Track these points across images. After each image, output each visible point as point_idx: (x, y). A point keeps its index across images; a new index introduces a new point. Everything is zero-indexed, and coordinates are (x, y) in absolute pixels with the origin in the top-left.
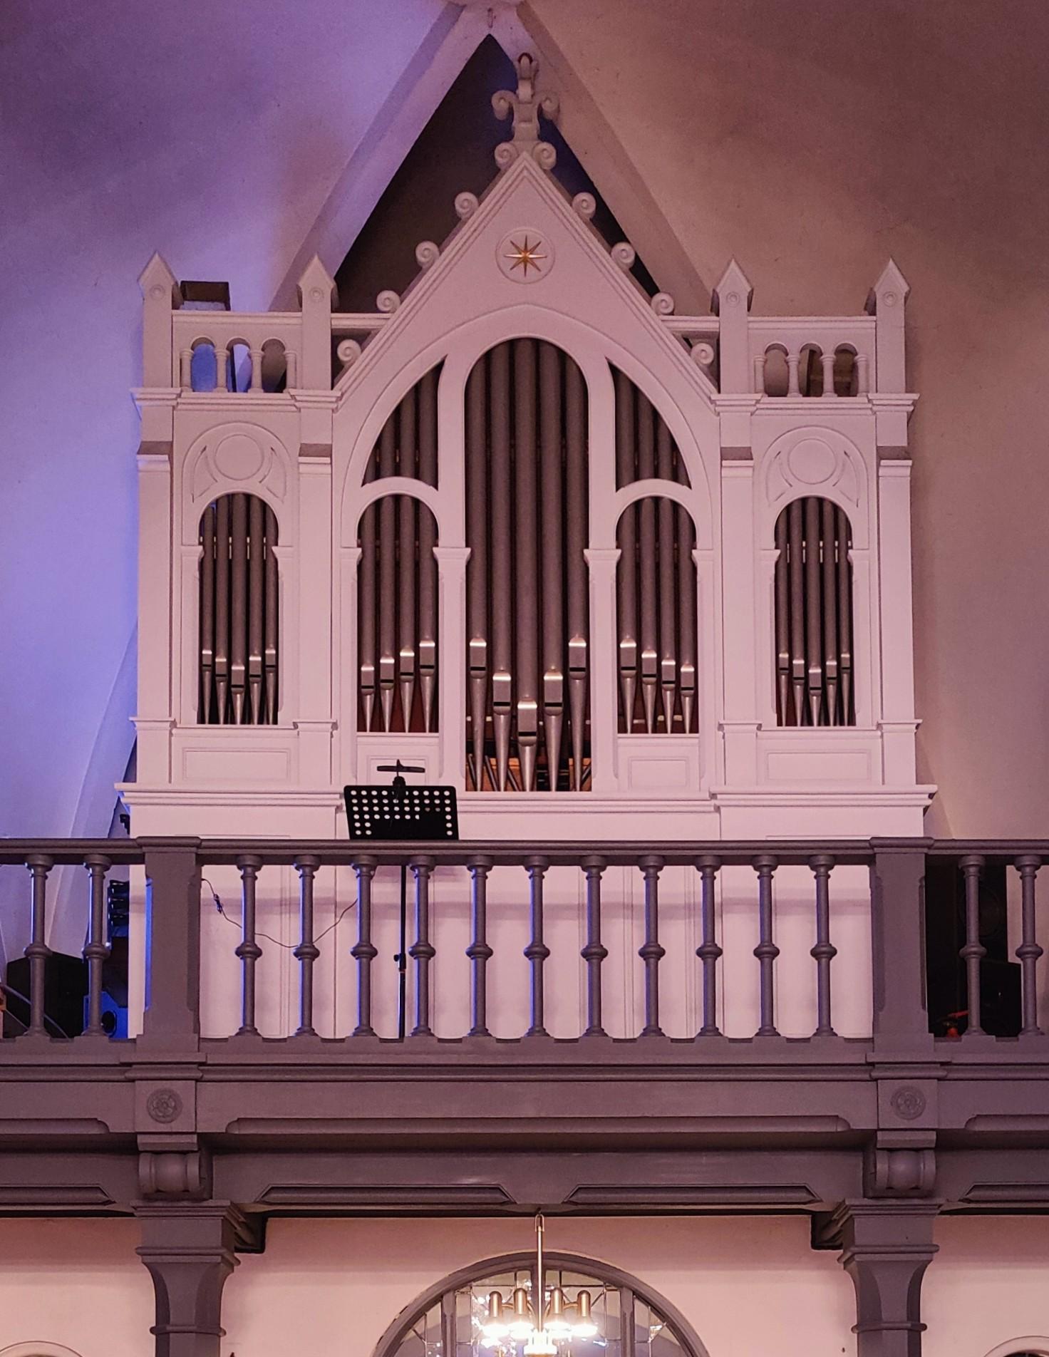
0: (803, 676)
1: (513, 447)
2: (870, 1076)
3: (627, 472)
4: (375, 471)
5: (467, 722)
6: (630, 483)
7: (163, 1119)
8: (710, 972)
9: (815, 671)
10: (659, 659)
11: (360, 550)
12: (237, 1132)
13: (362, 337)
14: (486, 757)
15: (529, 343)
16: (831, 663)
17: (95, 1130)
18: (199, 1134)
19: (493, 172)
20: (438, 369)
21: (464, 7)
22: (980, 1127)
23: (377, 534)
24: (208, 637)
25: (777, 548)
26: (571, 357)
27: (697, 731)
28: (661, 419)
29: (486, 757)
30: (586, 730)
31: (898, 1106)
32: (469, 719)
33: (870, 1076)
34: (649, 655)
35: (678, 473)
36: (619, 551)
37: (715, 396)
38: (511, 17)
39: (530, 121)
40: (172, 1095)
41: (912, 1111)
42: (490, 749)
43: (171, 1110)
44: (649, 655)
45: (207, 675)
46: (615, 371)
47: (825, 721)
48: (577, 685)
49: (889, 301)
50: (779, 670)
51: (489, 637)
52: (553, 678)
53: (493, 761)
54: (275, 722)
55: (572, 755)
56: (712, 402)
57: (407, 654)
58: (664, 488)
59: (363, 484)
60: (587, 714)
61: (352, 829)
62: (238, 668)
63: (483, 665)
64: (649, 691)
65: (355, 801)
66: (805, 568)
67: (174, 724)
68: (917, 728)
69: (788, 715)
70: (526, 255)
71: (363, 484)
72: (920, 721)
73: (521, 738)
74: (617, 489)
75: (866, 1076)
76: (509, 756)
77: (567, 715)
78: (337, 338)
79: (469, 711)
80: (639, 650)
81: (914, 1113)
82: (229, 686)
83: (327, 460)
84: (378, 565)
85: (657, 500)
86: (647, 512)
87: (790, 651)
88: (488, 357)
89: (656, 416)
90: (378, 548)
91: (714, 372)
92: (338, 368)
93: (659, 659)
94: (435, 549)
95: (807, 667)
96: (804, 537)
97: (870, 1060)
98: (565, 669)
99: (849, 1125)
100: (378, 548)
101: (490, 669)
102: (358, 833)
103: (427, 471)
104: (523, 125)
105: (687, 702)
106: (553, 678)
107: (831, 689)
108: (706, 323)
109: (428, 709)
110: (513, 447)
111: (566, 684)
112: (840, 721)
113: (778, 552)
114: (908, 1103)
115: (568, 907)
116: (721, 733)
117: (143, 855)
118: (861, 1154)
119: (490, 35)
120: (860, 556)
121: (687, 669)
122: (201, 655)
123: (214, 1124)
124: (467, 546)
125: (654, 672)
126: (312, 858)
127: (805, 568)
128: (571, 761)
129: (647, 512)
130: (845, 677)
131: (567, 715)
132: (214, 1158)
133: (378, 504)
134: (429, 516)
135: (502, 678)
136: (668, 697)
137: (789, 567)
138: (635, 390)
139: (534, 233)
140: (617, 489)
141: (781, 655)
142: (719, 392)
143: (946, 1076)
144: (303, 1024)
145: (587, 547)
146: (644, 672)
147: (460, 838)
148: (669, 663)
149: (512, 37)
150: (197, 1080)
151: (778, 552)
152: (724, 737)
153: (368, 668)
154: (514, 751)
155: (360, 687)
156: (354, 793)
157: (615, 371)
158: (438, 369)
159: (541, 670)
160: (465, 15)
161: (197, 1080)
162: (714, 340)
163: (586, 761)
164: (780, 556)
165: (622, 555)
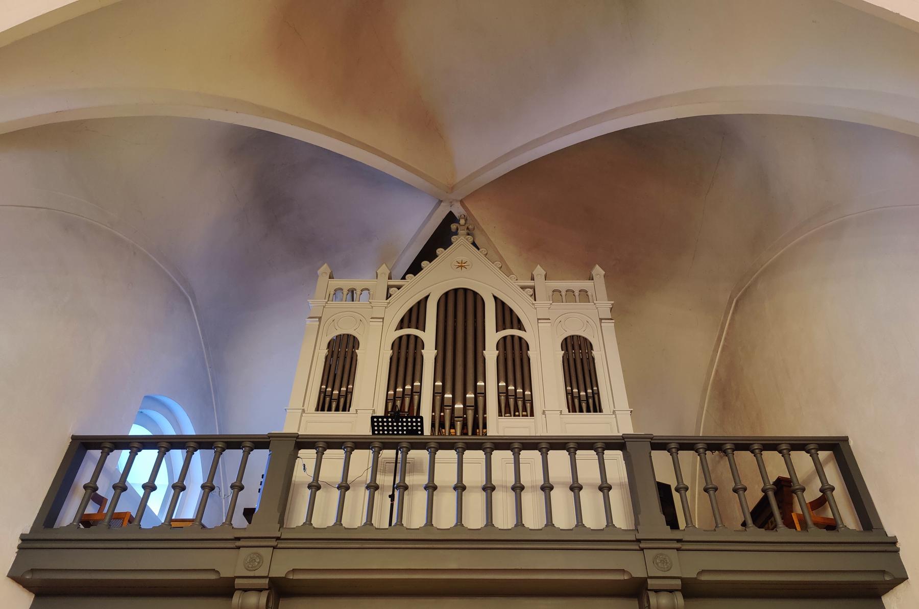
0: (578, 396)
1: (455, 322)
2: (639, 547)
3: (501, 325)
4: (401, 326)
5: (432, 415)
6: (501, 330)
7: (251, 569)
8: (549, 510)
9: (583, 393)
10: (516, 389)
11: (392, 351)
12: (291, 578)
13: (399, 288)
14: (441, 428)
15: (462, 290)
16: (589, 391)
17: (213, 577)
18: (270, 578)
19: (450, 243)
20: (427, 297)
21: (442, 201)
22: (704, 578)
23: (400, 348)
24: (325, 381)
25: (562, 350)
26: (478, 294)
27: (533, 416)
28: (513, 311)
29: (441, 428)
30: (485, 419)
31: (657, 564)
32: (433, 414)
33: (639, 547)
34: (511, 388)
35: (521, 327)
36: (498, 351)
37: (534, 302)
38: (458, 205)
39: (464, 230)
40: (259, 555)
41: (666, 567)
42: (442, 425)
43: (256, 564)
44: (511, 388)
45: (322, 395)
46: (495, 298)
47: (588, 411)
48: (481, 399)
49: (598, 276)
50: (567, 394)
51: (443, 382)
52: (470, 395)
53: (443, 431)
54: (349, 411)
55: (478, 428)
56: (533, 304)
57: (408, 387)
58: (516, 332)
59: (396, 330)
60: (485, 412)
61: (373, 431)
62: (336, 392)
63: (441, 392)
64: (512, 401)
65: (376, 428)
66: (575, 360)
67: (303, 411)
68: (631, 412)
69: (572, 408)
70: (461, 265)
71: (396, 330)
72: (632, 409)
73: (456, 419)
74: (497, 332)
75: (637, 548)
76: (450, 428)
77: (476, 412)
78: (389, 287)
79: (433, 411)
80: (507, 386)
81: (667, 568)
82: (331, 399)
83: (382, 320)
84: (398, 359)
85: (513, 336)
86: (509, 341)
87: (571, 386)
88: (446, 294)
89: (511, 311)
90: (399, 353)
91: (534, 296)
92: (388, 296)
93: (516, 389)
94: (422, 351)
95: (579, 392)
96: (573, 349)
97: (638, 537)
98: (475, 393)
99: (631, 576)
100: (399, 353)
101: (443, 393)
102: (376, 432)
103: (420, 324)
104: (461, 231)
105: (528, 405)
106: (470, 395)
107: (591, 401)
108: (531, 283)
109: (415, 408)
110: (455, 322)
111: (476, 398)
112: (595, 411)
113: (563, 352)
114: (663, 562)
115: (477, 487)
116: (544, 416)
117: (269, 442)
118: (637, 599)
119: (451, 211)
120: (597, 353)
121: (528, 393)
122: (321, 388)
123: (279, 571)
124: (436, 349)
125: (514, 394)
126: (351, 443)
127: (575, 360)
128: (478, 431)
129: (509, 341)
130: (596, 396)
131: (476, 412)
132: (281, 599)
133: (400, 338)
134: (421, 341)
135: (448, 396)
136: (520, 403)
137: (568, 360)
138: (503, 304)
139: (464, 259)
140: (497, 332)
141: (568, 388)
142: (535, 300)
143: (681, 548)
144: (336, 521)
145: (485, 350)
146: (509, 394)
147: (424, 434)
148: (520, 390)
149: (458, 211)
150: (274, 548)
151: (563, 352)
152: (545, 417)
153: (391, 392)
154: (453, 426)
155: (387, 399)
156: (375, 420)
157: (495, 298)
158: (427, 297)
159: (465, 393)
160: (442, 204)
161: (274, 548)
162: (533, 288)
163: (485, 431)
164: (564, 354)
165: (499, 353)
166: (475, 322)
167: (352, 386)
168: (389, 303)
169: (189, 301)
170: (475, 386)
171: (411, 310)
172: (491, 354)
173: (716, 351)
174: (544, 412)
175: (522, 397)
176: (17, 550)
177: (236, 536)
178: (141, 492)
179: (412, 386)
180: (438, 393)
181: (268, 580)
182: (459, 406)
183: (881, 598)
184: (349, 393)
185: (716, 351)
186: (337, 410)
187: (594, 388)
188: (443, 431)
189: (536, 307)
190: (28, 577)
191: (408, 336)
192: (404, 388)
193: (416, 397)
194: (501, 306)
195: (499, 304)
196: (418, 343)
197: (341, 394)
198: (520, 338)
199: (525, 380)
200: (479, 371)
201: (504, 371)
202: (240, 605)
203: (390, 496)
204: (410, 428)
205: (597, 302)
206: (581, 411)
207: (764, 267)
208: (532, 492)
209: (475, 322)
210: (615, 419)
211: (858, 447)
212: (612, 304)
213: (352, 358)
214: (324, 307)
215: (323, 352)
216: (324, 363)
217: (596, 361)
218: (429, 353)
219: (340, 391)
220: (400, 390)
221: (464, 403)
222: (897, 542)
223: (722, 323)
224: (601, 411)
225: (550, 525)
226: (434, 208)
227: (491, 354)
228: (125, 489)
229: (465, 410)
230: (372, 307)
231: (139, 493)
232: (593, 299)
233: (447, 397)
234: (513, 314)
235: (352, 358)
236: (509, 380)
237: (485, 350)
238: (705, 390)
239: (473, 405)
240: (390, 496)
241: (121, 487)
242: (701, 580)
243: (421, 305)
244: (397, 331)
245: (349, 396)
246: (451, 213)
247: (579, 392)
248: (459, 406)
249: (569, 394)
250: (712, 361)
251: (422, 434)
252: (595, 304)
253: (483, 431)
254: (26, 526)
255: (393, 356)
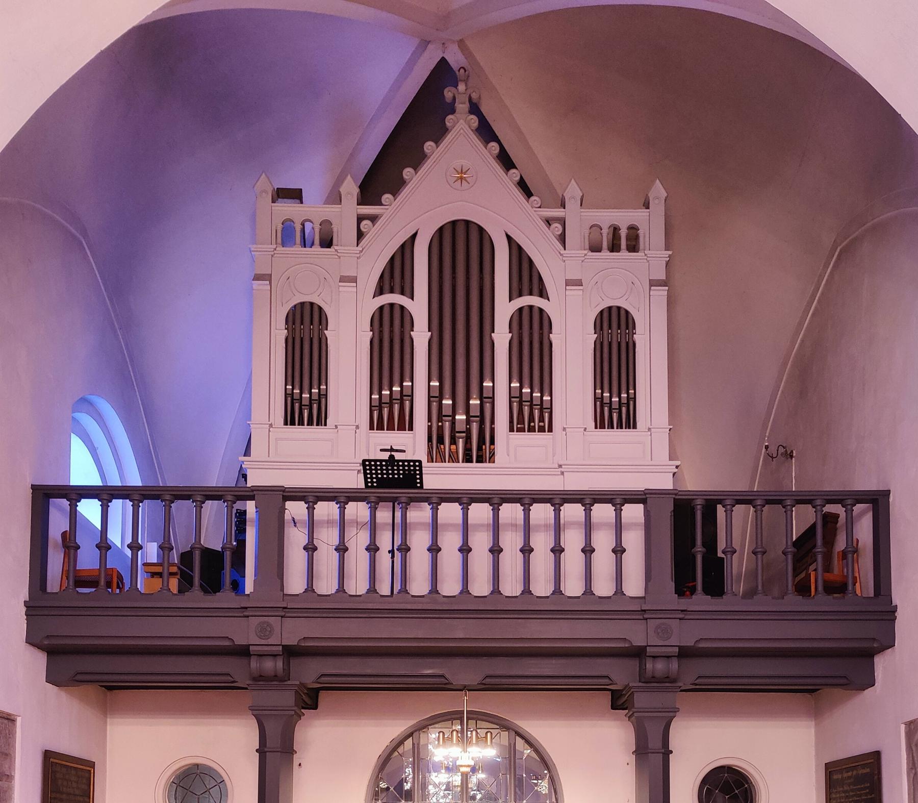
0: (609, 402)
1: (454, 278)
3: (515, 292)
4: (380, 291)
5: (428, 425)
6: (516, 298)
7: (264, 638)
10: (532, 393)
11: (372, 333)
12: (303, 645)
14: (439, 445)
15: (463, 222)
16: (624, 395)
17: (227, 643)
18: (283, 645)
19: (444, 131)
20: (414, 236)
24: (290, 379)
28: (533, 263)
29: (439, 445)
34: (526, 390)
35: (543, 293)
37: (563, 252)
39: (465, 103)
40: (269, 625)
42: (441, 440)
44: (526, 390)
46: (509, 238)
47: (620, 426)
48: (488, 406)
49: (657, 201)
50: (596, 399)
52: (475, 402)
53: (442, 447)
54: (325, 425)
55: (484, 444)
56: (561, 255)
57: (396, 389)
58: (535, 301)
59: (374, 298)
60: (492, 422)
61: (366, 483)
62: (306, 396)
64: (526, 410)
65: (368, 468)
67: (271, 426)
68: (670, 430)
69: (600, 424)
70: (462, 176)
71: (374, 298)
74: (510, 301)
76: (451, 444)
78: (360, 219)
79: (430, 420)
80: (521, 387)
82: (301, 405)
85: (531, 307)
88: (441, 230)
89: (531, 262)
90: (381, 332)
91: (562, 239)
92: (360, 235)
93: (532, 393)
94: (412, 333)
95: (611, 397)
98: (481, 398)
100: (381, 332)
101: (441, 397)
102: (370, 484)
104: (461, 105)
105: (546, 415)
106: (475, 402)
107: (624, 409)
108: (558, 213)
109: (407, 418)
110: (454, 278)
111: (482, 406)
113: (596, 335)
115: (482, 525)
118: (638, 659)
122: (286, 389)
125: (529, 399)
127: (610, 344)
128: (484, 447)
130: (631, 403)
135: (447, 402)
137: (602, 344)
139: (466, 163)
140: (510, 301)
145: (494, 332)
146: (524, 400)
147: (424, 488)
148: (537, 395)
149: (455, 59)
151: (596, 335)
153: (375, 396)
154: (453, 441)
156: (367, 463)
157: (509, 238)
158: (414, 236)
159: (468, 398)
161: (282, 617)
166: (481, 279)
167: (325, 387)
168: (361, 251)
169: (81, 243)
170: (481, 388)
171: (392, 259)
172: (502, 337)
173: (806, 311)
174: (564, 429)
175: (539, 403)
176: (25, 617)
177: (242, 606)
178: (129, 553)
179: (401, 386)
180: (434, 398)
181: (281, 647)
182: (461, 417)
183: (874, 657)
184: (323, 396)
185: (806, 311)
186: (310, 423)
187: (630, 391)
188: (442, 447)
189: (564, 259)
190: (46, 643)
191: (392, 305)
192: (391, 391)
193: (407, 403)
194: (517, 252)
195: (515, 252)
196: (404, 317)
197: (313, 398)
198: (541, 311)
199: (545, 382)
200: (486, 369)
201: (517, 370)
202: (258, 669)
203: (389, 552)
204: (407, 472)
205: (650, 252)
206: (611, 426)
207: (875, 220)
208: (545, 532)
209: (481, 279)
210: (650, 437)
211: (898, 506)
212: (670, 256)
213: (320, 340)
214: (272, 256)
215: (281, 334)
216: (284, 350)
217: (636, 350)
218: (421, 336)
219: (310, 393)
220: (386, 392)
221: (467, 412)
222: (896, 611)
223: (820, 275)
224: (635, 427)
225: (557, 592)
226: (414, 52)
227: (502, 337)
228: (109, 548)
229: (468, 422)
230: (339, 257)
231: (97, 526)
232: (645, 247)
233: (445, 404)
234: (534, 270)
235: (320, 340)
236: (524, 380)
237: (494, 332)
238: (785, 364)
239: (479, 414)
240: (389, 552)
241: (104, 546)
242: (699, 647)
243: (407, 248)
244: (376, 298)
245: (323, 400)
246: (443, 61)
247: (611, 397)
248: (461, 417)
249: (598, 400)
250: (801, 324)
251: (422, 487)
252: (645, 255)
253: (490, 447)
254: (24, 595)
255: (374, 339)
